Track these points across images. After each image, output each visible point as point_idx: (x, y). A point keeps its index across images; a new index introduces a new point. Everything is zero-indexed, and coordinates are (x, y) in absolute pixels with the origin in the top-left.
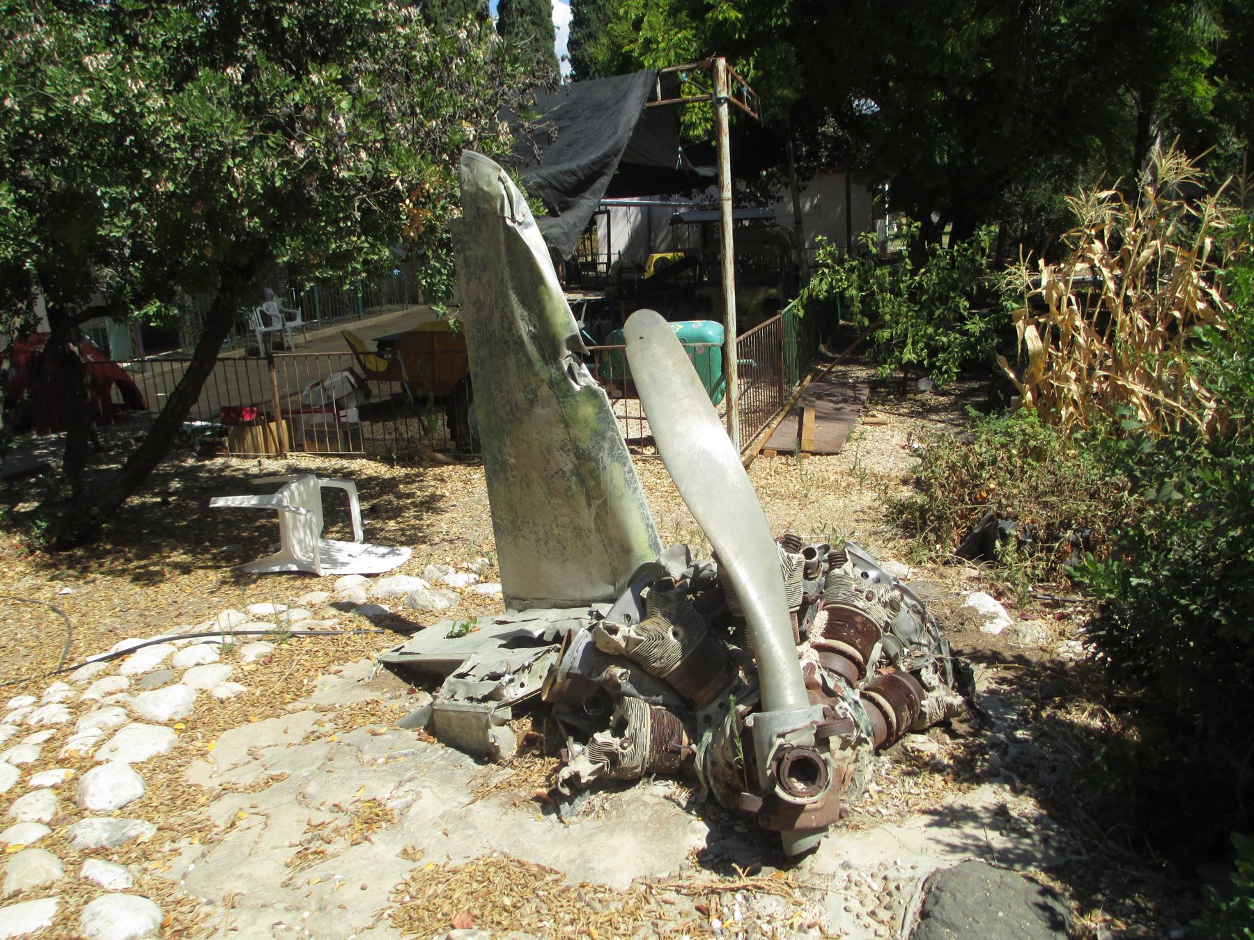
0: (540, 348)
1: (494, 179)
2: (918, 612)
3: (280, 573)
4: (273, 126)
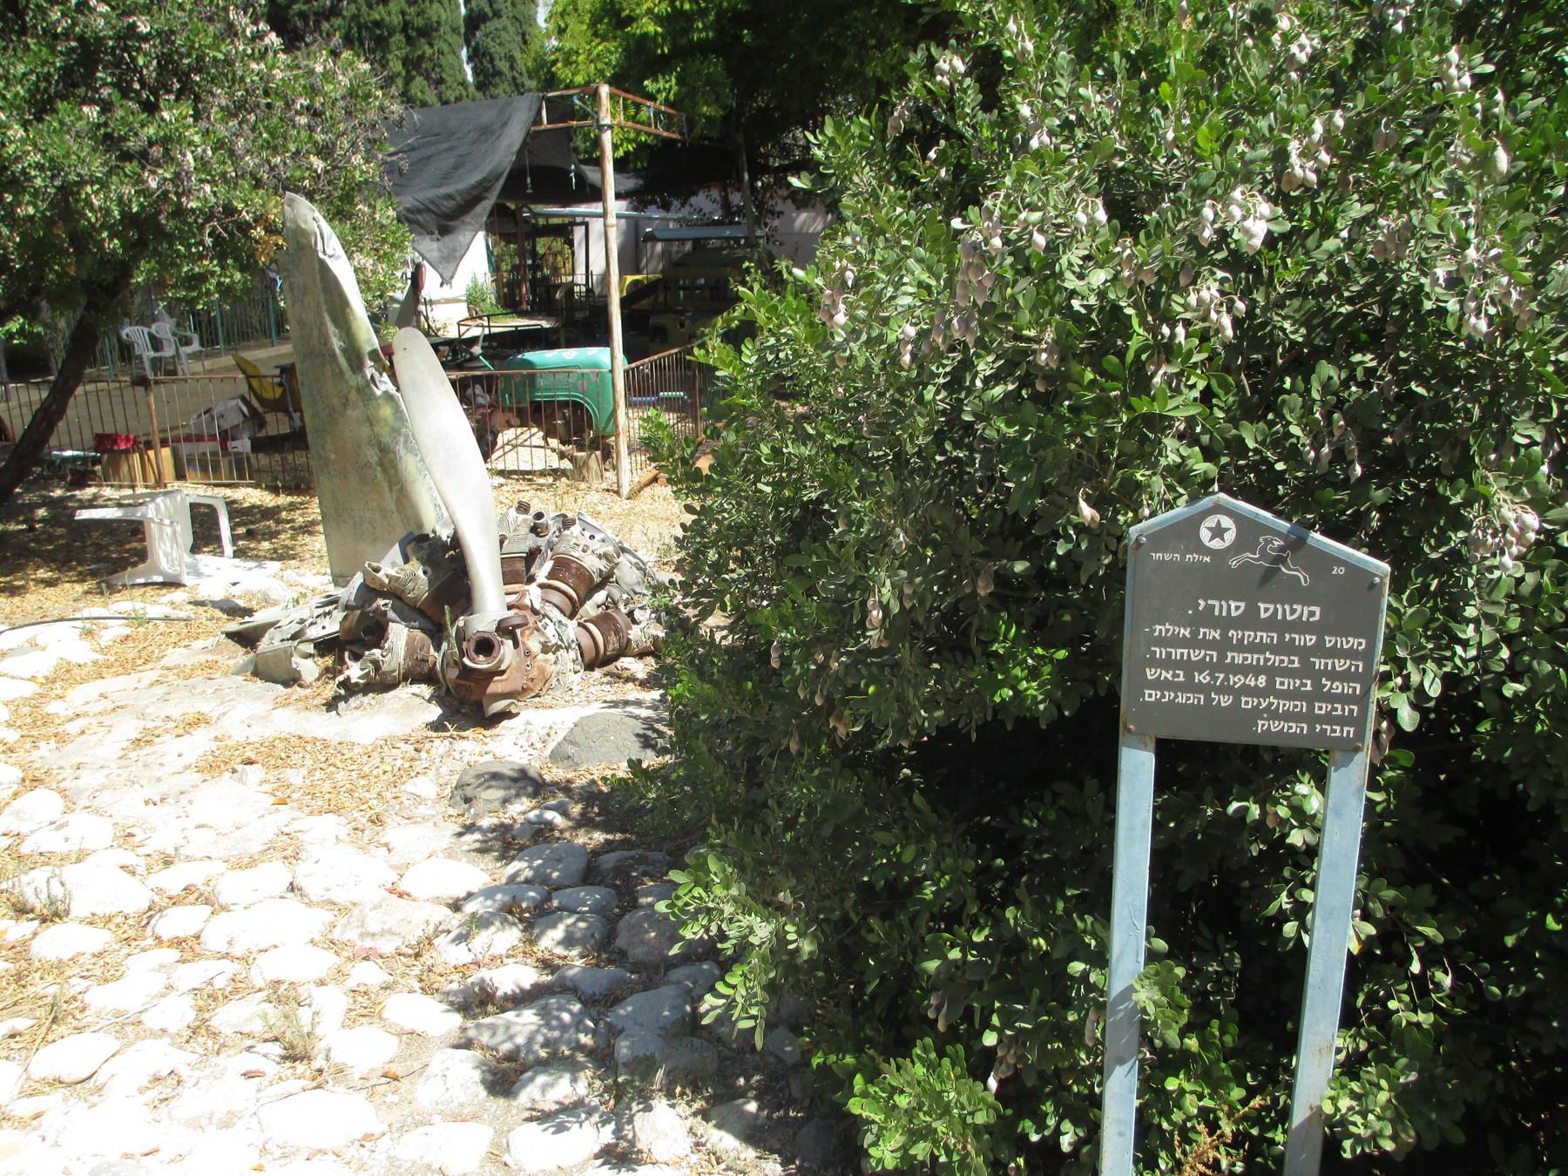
0: (349, 360)
1: (310, 219)
2: (639, 569)
3: (145, 585)
4: (127, 156)
